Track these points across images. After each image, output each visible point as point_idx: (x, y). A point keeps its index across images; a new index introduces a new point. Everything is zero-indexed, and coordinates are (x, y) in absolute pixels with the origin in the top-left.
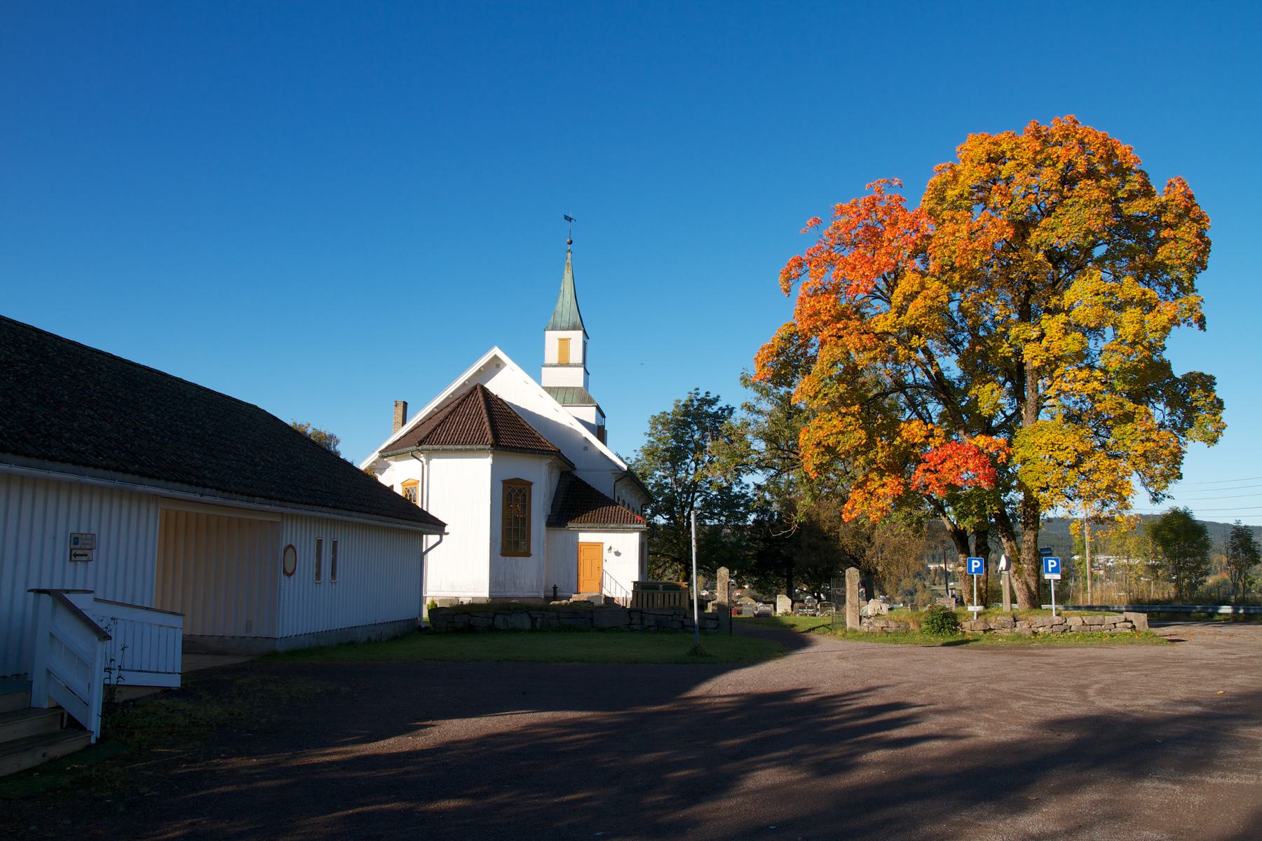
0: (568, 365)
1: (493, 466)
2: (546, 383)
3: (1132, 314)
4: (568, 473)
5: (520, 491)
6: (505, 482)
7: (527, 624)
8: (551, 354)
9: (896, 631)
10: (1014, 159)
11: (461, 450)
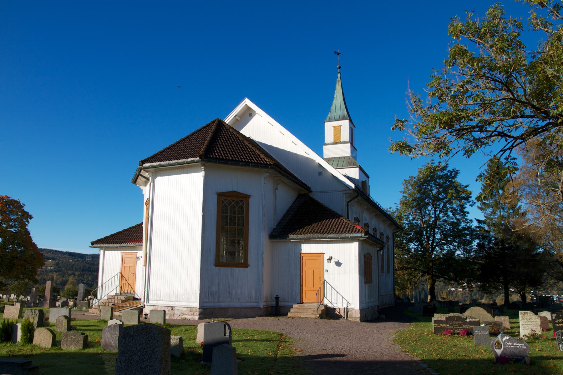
0: (340, 143)
2: (326, 156)
5: (237, 203)
6: (220, 195)
8: (329, 136)
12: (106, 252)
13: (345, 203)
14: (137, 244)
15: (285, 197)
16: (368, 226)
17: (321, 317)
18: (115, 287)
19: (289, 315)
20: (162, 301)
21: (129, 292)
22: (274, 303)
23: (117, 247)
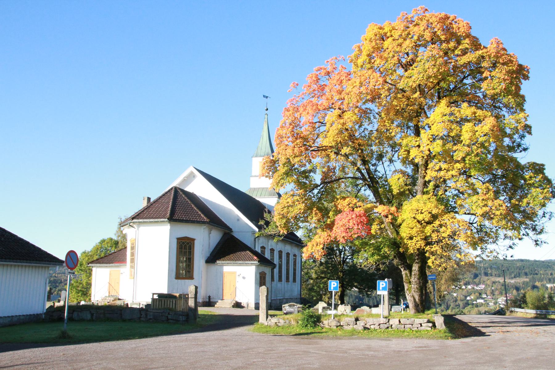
1: (171, 230)
3: (467, 126)
4: (228, 233)
5: (188, 243)
7: (89, 317)
9: (283, 326)
10: (392, 36)
11: (151, 222)
13: (253, 239)
15: (216, 236)
16: (274, 250)
17: (233, 307)
19: (216, 306)
22: (208, 300)
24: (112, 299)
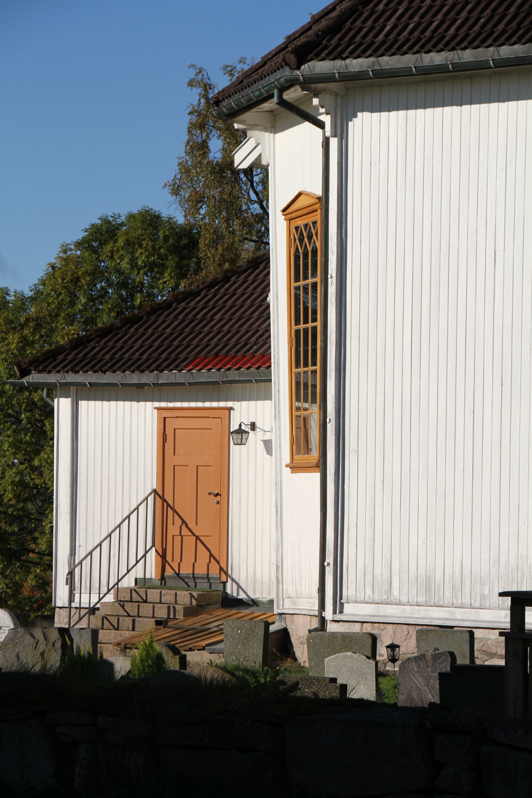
11: (429, 74)
12: (83, 404)
14: (233, 375)
18: (141, 553)
20: (399, 603)
21: (201, 570)
23: (140, 386)
24: (184, 598)
